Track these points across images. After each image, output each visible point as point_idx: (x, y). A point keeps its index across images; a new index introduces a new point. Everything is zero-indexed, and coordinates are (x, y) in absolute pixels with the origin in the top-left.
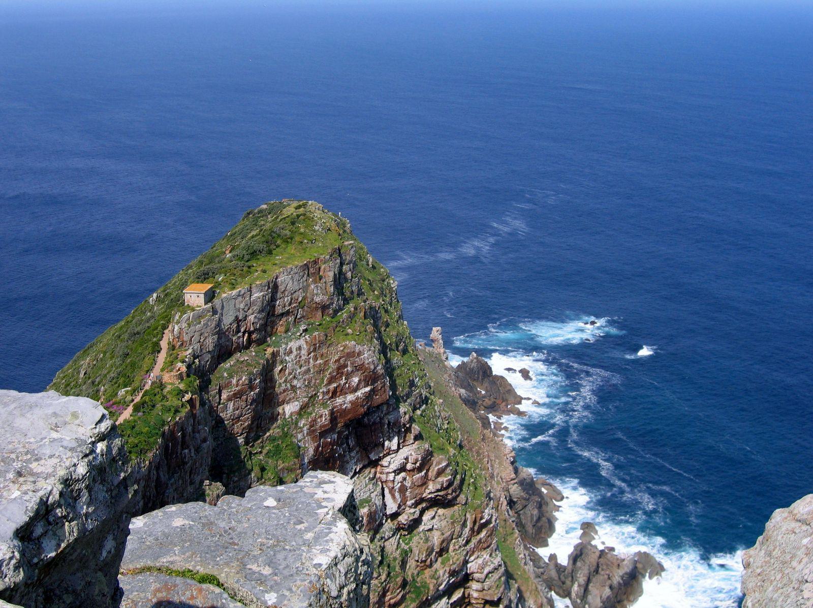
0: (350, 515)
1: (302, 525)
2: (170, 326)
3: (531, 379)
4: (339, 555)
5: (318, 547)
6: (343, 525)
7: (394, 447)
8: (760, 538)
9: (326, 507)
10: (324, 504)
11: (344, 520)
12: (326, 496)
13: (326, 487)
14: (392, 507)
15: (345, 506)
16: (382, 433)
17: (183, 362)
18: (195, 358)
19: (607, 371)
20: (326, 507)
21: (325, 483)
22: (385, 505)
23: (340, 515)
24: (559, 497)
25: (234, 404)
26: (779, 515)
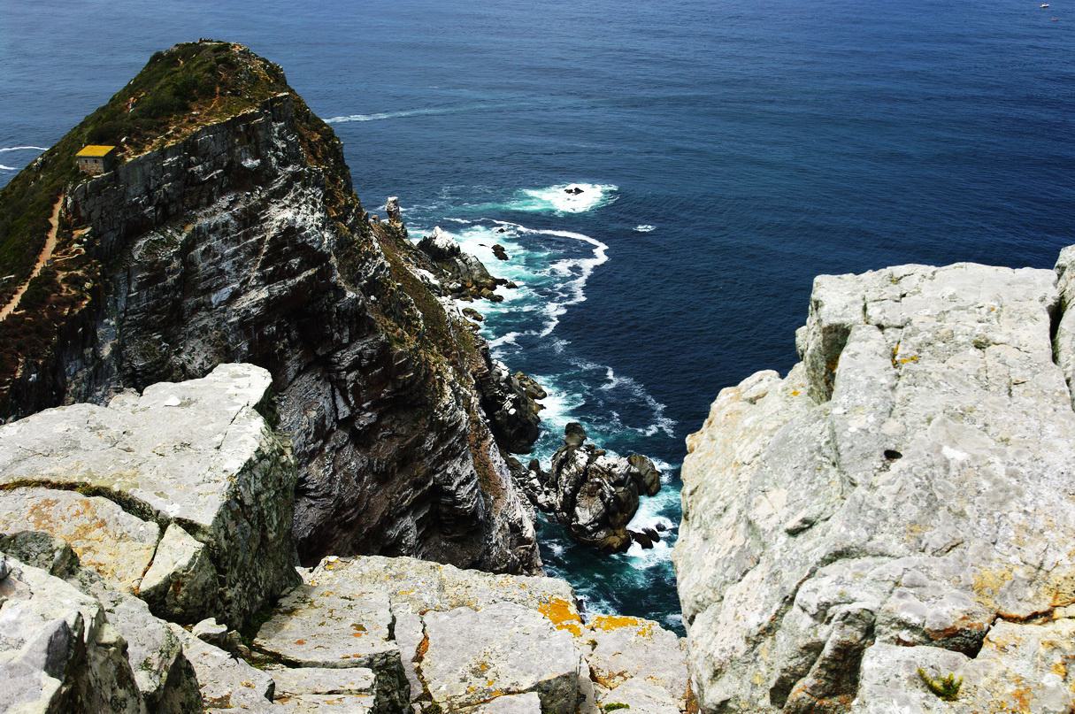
0: (269, 413)
1: (211, 425)
2: (62, 199)
3: (506, 258)
4: (254, 458)
5: (228, 450)
6: (259, 423)
7: (345, 341)
8: (706, 421)
9: (239, 404)
10: (236, 401)
11: (261, 419)
12: (238, 391)
13: (239, 381)
14: (344, 412)
15: (262, 402)
16: (330, 323)
17: (79, 242)
18: (96, 238)
19: (210, 202)
20: (239, 404)
21: (238, 376)
22: (336, 410)
23: (256, 413)
24: (540, 395)
25: (148, 293)
26: (725, 394)
